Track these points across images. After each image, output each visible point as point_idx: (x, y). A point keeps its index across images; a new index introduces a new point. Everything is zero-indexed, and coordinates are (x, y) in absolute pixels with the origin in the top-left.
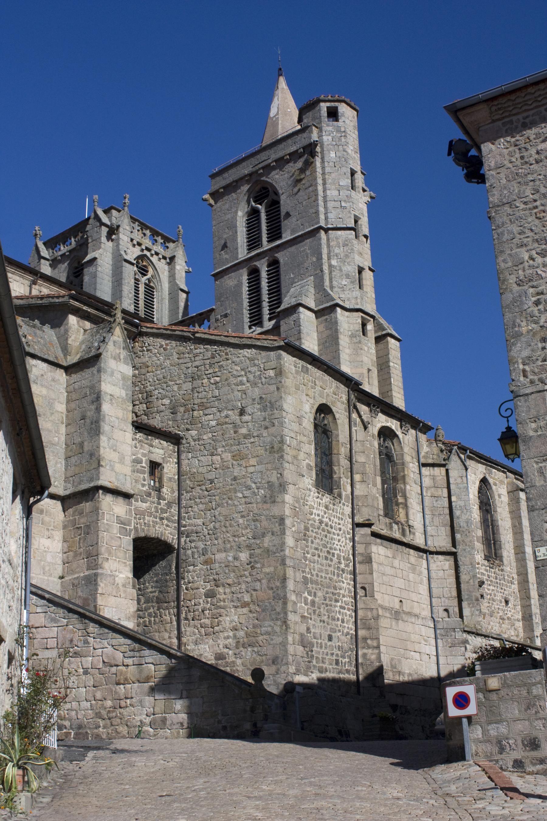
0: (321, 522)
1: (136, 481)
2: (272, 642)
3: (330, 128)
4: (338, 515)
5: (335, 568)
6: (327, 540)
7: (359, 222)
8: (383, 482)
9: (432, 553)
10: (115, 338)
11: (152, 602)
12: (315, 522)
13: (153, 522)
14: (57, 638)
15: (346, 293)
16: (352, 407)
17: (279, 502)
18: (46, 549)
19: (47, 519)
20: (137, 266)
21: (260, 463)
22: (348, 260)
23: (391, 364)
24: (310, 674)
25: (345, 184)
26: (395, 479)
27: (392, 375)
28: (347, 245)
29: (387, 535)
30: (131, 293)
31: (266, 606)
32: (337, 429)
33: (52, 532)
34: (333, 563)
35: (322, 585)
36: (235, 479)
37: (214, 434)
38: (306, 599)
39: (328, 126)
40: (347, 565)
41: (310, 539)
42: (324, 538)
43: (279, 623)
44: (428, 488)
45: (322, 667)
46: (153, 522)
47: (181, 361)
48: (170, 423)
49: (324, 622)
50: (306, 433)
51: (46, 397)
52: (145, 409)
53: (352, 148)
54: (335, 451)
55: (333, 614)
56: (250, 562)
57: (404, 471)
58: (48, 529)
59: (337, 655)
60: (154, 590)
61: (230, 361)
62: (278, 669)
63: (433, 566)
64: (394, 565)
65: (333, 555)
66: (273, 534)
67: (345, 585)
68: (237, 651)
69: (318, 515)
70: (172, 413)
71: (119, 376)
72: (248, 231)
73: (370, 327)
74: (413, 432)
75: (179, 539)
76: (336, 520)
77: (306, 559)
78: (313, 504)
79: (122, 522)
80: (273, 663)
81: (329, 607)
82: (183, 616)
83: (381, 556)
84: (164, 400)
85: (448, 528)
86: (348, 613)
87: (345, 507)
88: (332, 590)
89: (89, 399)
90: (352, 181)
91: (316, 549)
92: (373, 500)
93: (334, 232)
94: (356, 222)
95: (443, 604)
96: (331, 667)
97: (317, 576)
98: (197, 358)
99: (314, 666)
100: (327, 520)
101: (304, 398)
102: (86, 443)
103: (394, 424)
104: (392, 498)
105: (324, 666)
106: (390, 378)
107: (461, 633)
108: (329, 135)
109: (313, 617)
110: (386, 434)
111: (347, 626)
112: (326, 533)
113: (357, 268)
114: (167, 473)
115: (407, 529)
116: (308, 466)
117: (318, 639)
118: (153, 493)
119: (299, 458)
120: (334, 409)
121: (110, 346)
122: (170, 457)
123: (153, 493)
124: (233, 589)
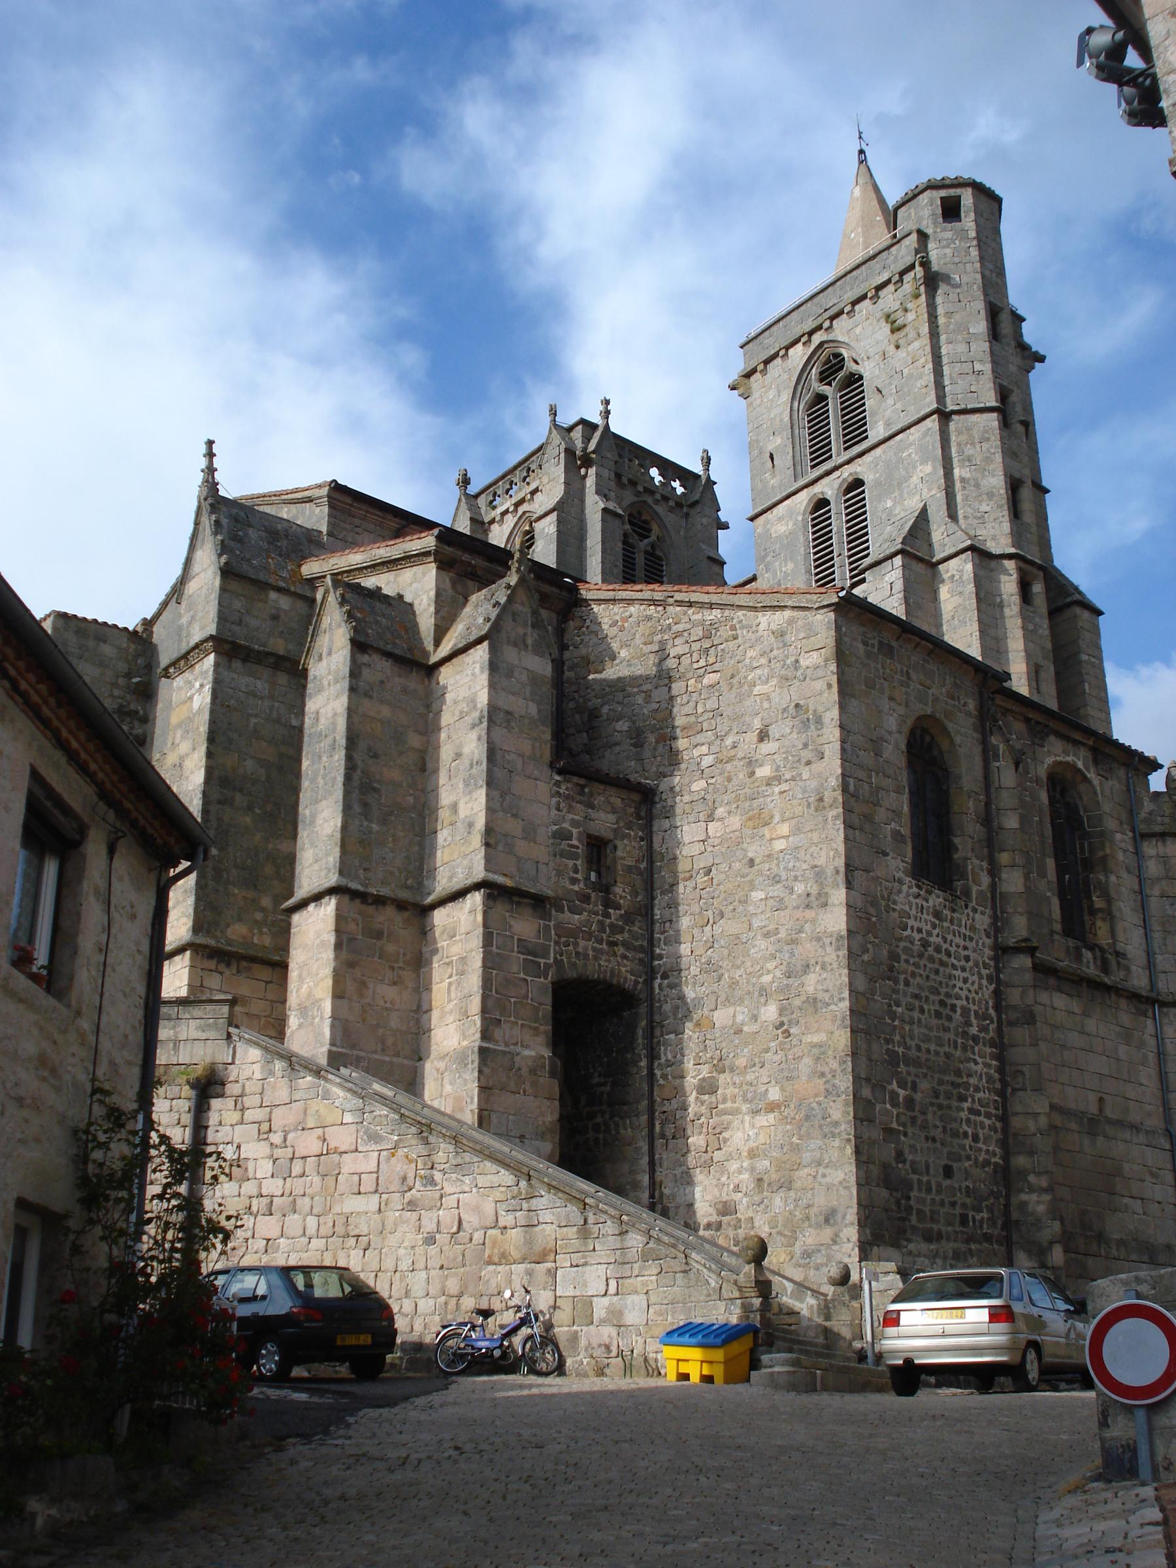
0: (925, 944)
1: (559, 873)
2: (824, 1181)
3: (949, 235)
4: (963, 930)
5: (957, 1035)
8: (1061, 870)
13: (594, 949)
15: (989, 526)
16: (986, 723)
18: (388, 1005)
19: (390, 948)
20: (631, 523)
23: (1084, 657)
24: (905, 1243)
26: (1088, 865)
27: (1086, 677)
28: (988, 439)
30: (616, 566)
31: (813, 1109)
34: (952, 1026)
35: (929, 1068)
36: (751, 862)
38: (894, 1095)
39: (944, 230)
40: (983, 1029)
42: (932, 976)
43: (837, 1143)
46: (594, 949)
49: (934, 1140)
52: (586, 741)
54: (956, 808)
56: (782, 1024)
57: (1103, 849)
58: (392, 968)
59: (964, 1205)
60: (602, 1080)
62: (837, 1235)
65: (953, 1008)
67: (979, 1068)
69: (920, 931)
70: (635, 745)
73: (1038, 588)
76: (957, 940)
77: (893, 1016)
78: (907, 908)
80: (827, 1221)
83: (1057, 1012)
84: (621, 723)
86: (987, 1122)
87: (978, 916)
88: (950, 1078)
93: (962, 417)
96: (950, 1229)
98: (677, 642)
99: (914, 1228)
100: (939, 940)
101: (885, 704)
106: (1083, 682)
108: (948, 246)
109: (910, 1131)
110: (1061, 784)
111: (984, 1147)
112: (937, 966)
115: (1112, 959)
116: (896, 835)
117: (921, 1174)
118: (593, 895)
120: (950, 726)
124: (750, 1077)
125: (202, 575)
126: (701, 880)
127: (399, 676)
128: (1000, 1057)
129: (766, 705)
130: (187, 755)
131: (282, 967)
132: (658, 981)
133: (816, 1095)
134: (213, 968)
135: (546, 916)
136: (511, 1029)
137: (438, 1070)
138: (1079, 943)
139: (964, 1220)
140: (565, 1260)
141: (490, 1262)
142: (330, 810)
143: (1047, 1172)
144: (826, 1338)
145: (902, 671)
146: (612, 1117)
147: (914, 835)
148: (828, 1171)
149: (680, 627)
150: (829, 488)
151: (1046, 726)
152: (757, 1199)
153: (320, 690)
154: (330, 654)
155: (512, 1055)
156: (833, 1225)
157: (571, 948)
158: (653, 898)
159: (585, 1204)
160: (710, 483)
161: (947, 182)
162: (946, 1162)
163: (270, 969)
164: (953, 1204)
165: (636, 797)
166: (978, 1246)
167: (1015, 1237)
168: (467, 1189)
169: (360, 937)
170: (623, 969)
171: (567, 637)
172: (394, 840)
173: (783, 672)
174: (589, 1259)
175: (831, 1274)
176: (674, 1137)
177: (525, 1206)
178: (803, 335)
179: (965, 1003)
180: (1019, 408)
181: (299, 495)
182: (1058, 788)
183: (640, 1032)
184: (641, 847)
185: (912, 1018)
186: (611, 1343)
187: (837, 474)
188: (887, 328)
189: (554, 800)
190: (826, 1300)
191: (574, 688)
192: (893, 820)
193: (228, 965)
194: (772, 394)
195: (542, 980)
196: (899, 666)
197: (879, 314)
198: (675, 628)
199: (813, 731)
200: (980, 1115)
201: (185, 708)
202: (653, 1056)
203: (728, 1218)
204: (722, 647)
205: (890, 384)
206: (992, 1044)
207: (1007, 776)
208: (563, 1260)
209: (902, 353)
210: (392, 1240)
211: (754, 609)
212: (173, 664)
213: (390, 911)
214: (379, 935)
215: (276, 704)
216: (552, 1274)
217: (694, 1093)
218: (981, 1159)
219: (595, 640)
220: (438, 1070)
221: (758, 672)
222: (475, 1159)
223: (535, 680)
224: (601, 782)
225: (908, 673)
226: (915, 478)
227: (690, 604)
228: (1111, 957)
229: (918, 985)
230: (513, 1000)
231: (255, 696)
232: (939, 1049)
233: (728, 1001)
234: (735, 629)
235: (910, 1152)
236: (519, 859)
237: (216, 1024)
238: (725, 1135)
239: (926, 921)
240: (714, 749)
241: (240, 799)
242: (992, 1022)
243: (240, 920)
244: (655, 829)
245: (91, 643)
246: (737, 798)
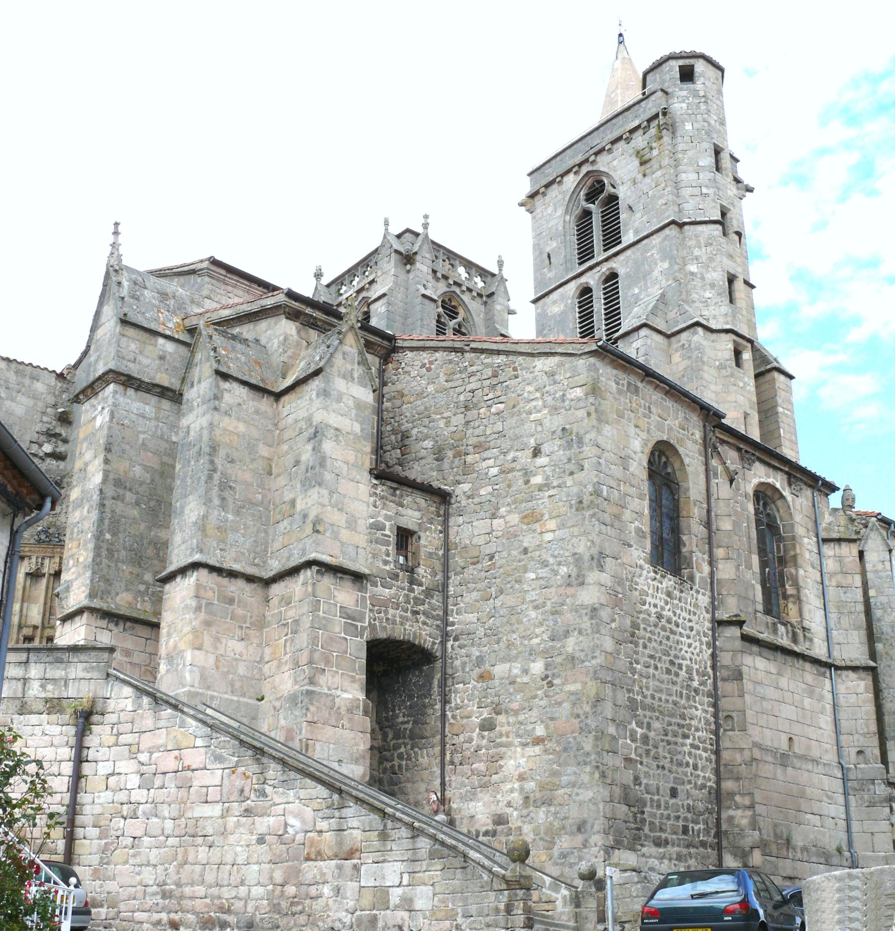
0: (660, 617)
1: (375, 556)
2: (577, 798)
3: (684, 93)
4: (688, 607)
5: (682, 687)
6: (670, 643)
7: (728, 215)
8: (763, 564)
9: (838, 668)
10: (346, 348)
11: (404, 737)
12: (649, 615)
13: (401, 617)
14: (221, 786)
15: (711, 308)
16: (709, 449)
17: (589, 584)
18: (237, 656)
20: (443, 307)
21: (561, 526)
22: (713, 265)
23: (780, 410)
24: (640, 847)
25: (707, 164)
26: (782, 561)
27: (781, 424)
28: (711, 244)
29: (769, 640)
31: (570, 743)
32: (686, 478)
33: (248, 631)
34: (679, 680)
35: (661, 712)
36: (525, 551)
37: (495, 487)
39: (681, 90)
40: (703, 683)
41: (641, 641)
42: (664, 641)
43: (588, 769)
44: (832, 575)
45: (659, 838)
46: (401, 617)
47: (450, 384)
48: (435, 473)
50: (634, 482)
51: (244, 435)
52: (399, 456)
53: (716, 118)
54: (684, 513)
55: (679, 757)
56: (547, 677)
57: (794, 548)
59: (686, 819)
60: (406, 719)
61: (519, 379)
62: (586, 841)
63: (841, 688)
64: (781, 685)
65: (680, 667)
66: (580, 633)
67: (699, 713)
68: (525, 812)
69: (655, 606)
70: (437, 460)
71: (351, 403)
72: (578, 240)
73: (747, 356)
74: (808, 492)
75: (443, 643)
76: (684, 614)
78: (646, 588)
79: (349, 616)
80: (579, 830)
81: (672, 746)
82: (448, 757)
83: (758, 672)
84: (426, 442)
85: (863, 633)
86: (704, 755)
87: (700, 597)
89: (306, 435)
90: (717, 161)
91: (652, 657)
92: (746, 589)
93: (692, 227)
94: (723, 214)
95: (856, 744)
97: (653, 697)
98: (472, 379)
99: (646, 836)
100: (671, 614)
101: (632, 430)
102: (298, 501)
103: (778, 481)
104: (776, 588)
105: (664, 836)
106: (779, 428)
107: (883, 786)
108: (683, 102)
109: (645, 760)
110: (764, 496)
111: (702, 774)
112: (668, 634)
113: (726, 275)
114: (425, 546)
115: (800, 632)
116: (639, 531)
117: (653, 794)
118: (401, 574)
119: (624, 518)
120: (681, 450)
121: (338, 360)
122: (432, 523)
123: (401, 574)
124: (521, 717)
125: (107, 324)
126: (486, 563)
127: (253, 400)
128: (715, 705)
129: (539, 428)
130: (90, 462)
131: (156, 626)
132: (451, 642)
133: (573, 732)
134: (105, 626)
135: (363, 589)
136: (333, 676)
137: (275, 708)
138: (776, 620)
139: (685, 830)
140: (368, 857)
141: (308, 859)
142: (196, 503)
143: (749, 794)
144: (577, 922)
145: (645, 406)
146: (412, 749)
147: (653, 532)
148: (580, 791)
149: (474, 368)
150: (593, 279)
151: (753, 454)
152: (525, 812)
153: (191, 410)
154: (199, 382)
155: (334, 697)
156: (584, 833)
157: (382, 615)
158: (448, 578)
159: (385, 813)
160: (503, 280)
161: (683, 54)
162: (672, 785)
163: (150, 629)
164: (677, 818)
165: (437, 499)
166: (695, 850)
167: (724, 843)
168: (291, 800)
169: (216, 602)
170: (424, 633)
171: (387, 375)
172: (245, 528)
173: (553, 403)
174: (387, 857)
175: (581, 871)
176: (461, 764)
177: (337, 814)
178: (574, 167)
179: (689, 662)
180: (735, 223)
181: (186, 269)
182: (761, 503)
183: (436, 683)
184: (439, 538)
185: (648, 673)
186: (403, 924)
187: (598, 268)
188: (636, 162)
189: (372, 499)
190: (576, 892)
191: (391, 415)
192: (636, 519)
193: (117, 624)
194: (550, 210)
195: (359, 639)
196: (643, 402)
197: (631, 151)
198: (470, 369)
199: (575, 449)
200: (699, 749)
201: (90, 426)
202: (445, 701)
203: (502, 826)
204: (506, 384)
205: (639, 202)
206: (709, 695)
207: (721, 488)
208: (368, 858)
209: (648, 180)
210: (232, 839)
211: (532, 355)
212: (83, 391)
213: (241, 583)
214: (231, 601)
215: (161, 425)
216: (356, 868)
217: (477, 730)
218: (699, 783)
219: (408, 378)
220: (275, 708)
221: (534, 403)
222: (299, 776)
223: (359, 405)
224: (410, 486)
225: (649, 408)
226: (656, 272)
227: (482, 351)
228: (799, 631)
229: (653, 647)
230: (335, 654)
231: (144, 417)
232: (668, 698)
233: (504, 660)
234: (516, 370)
235: (645, 777)
236: (343, 544)
237: (98, 667)
238: (501, 762)
239: (660, 599)
240: (499, 463)
241: (130, 497)
242: (709, 678)
243: (127, 590)
244: (451, 524)
245: (27, 381)
246: (515, 502)
